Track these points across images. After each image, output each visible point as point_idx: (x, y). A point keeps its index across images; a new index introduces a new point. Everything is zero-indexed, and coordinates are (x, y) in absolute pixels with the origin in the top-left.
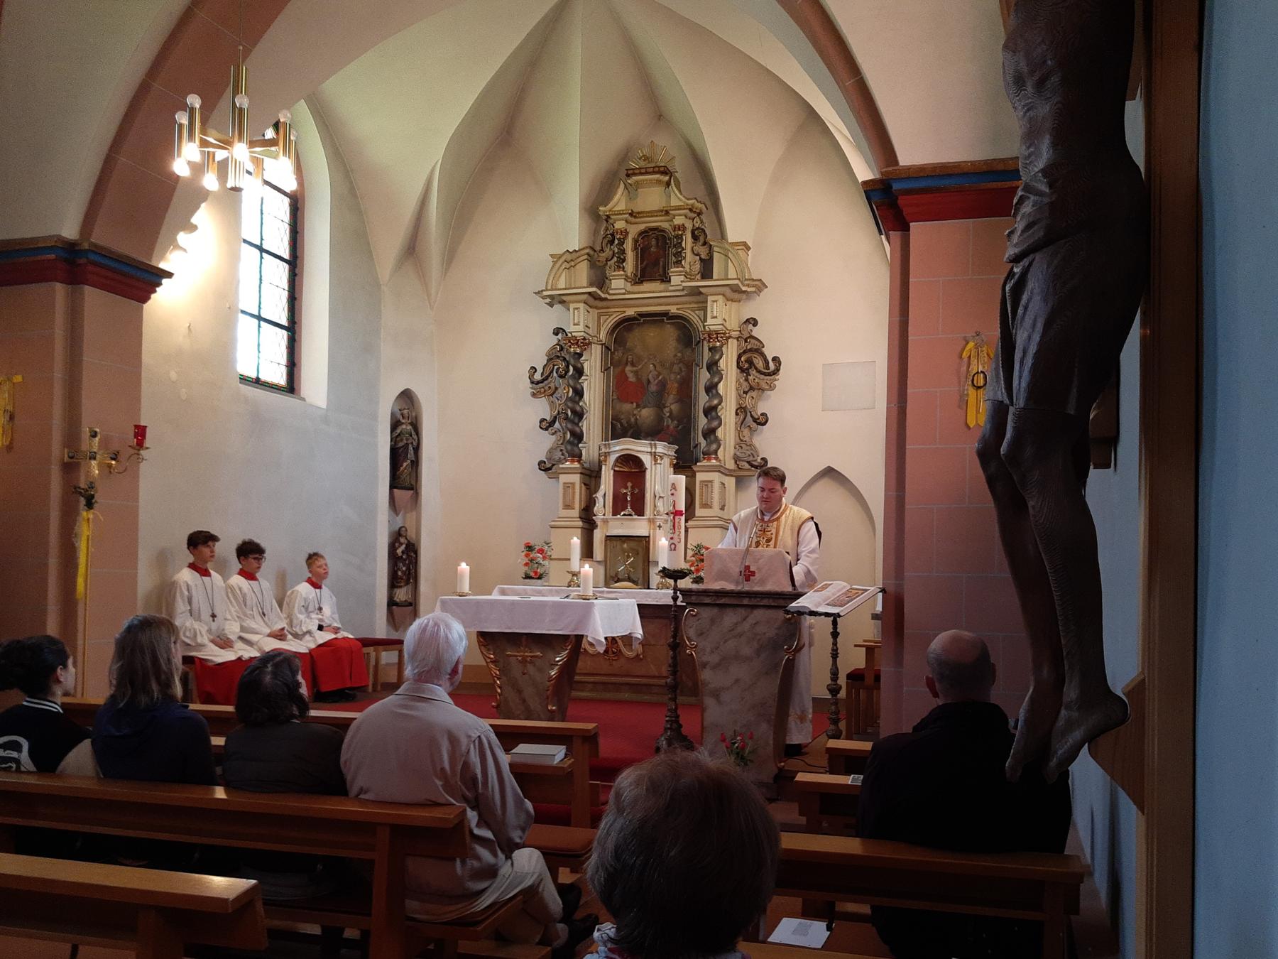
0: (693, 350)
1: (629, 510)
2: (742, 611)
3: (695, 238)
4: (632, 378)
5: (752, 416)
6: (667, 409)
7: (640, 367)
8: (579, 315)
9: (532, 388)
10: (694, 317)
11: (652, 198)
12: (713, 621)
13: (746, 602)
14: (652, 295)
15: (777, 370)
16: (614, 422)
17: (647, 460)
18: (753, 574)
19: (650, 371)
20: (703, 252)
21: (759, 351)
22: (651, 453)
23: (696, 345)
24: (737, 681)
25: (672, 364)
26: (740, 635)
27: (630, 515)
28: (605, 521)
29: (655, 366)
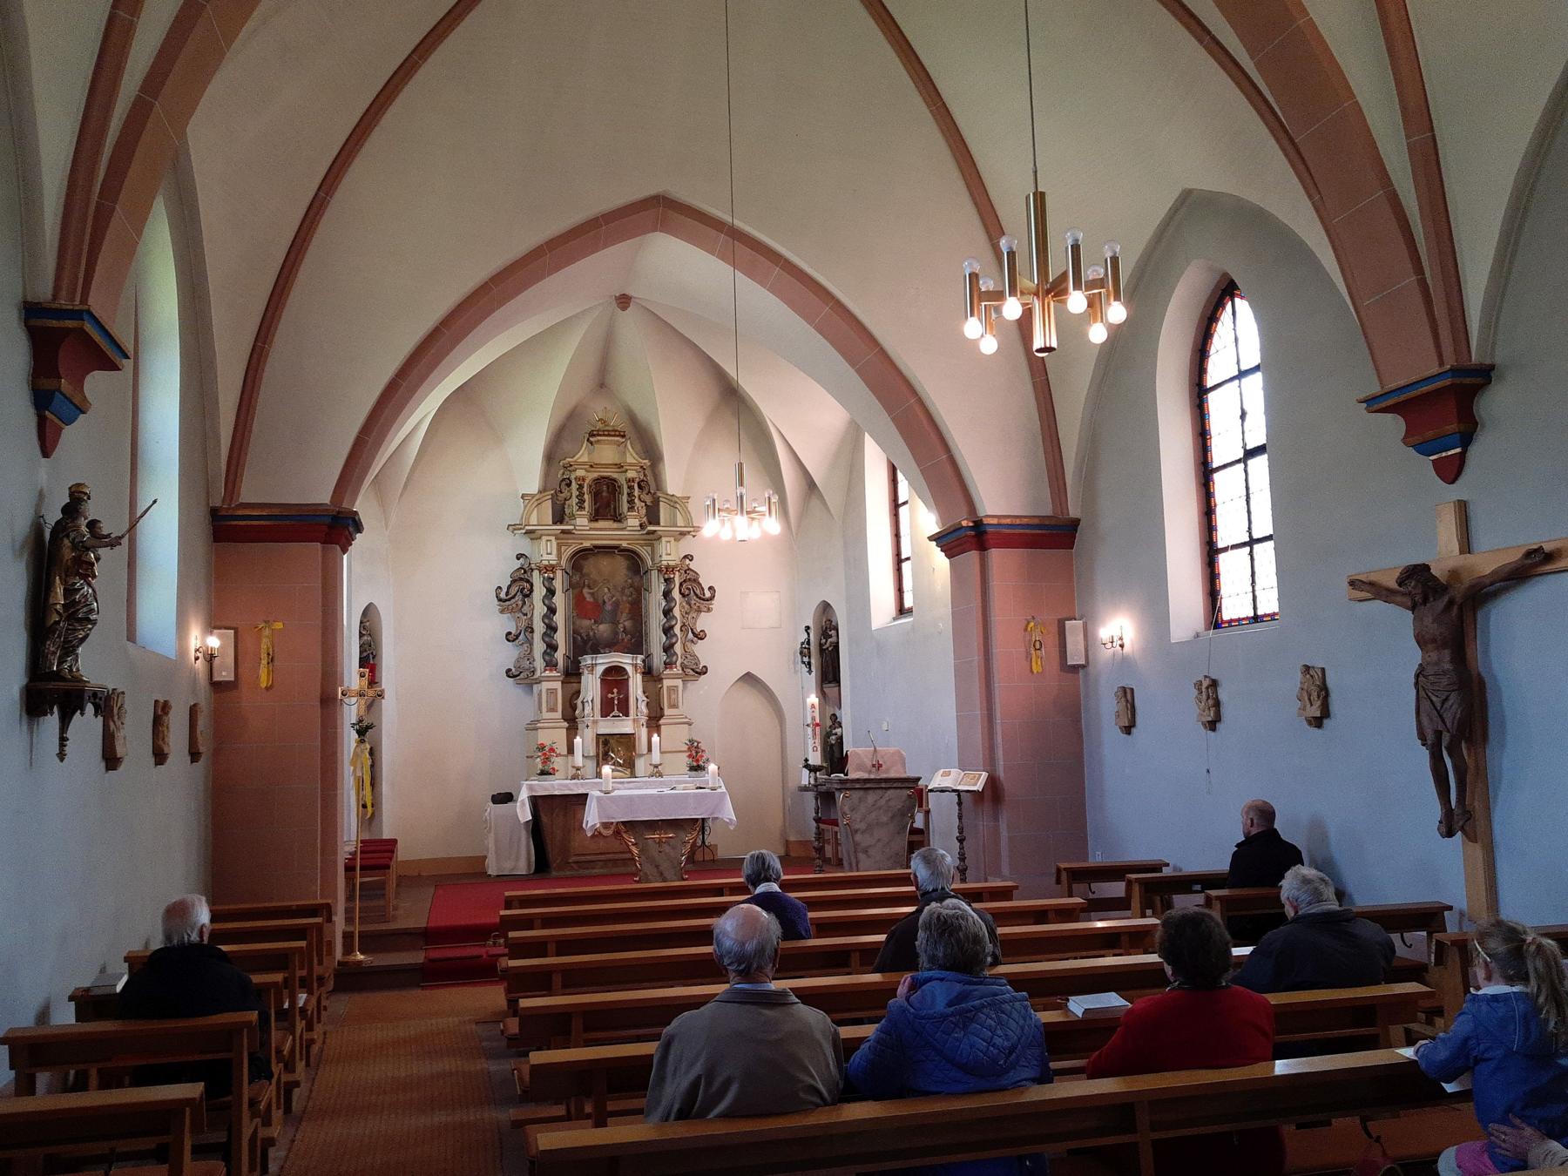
0: (642, 577)
1: (616, 712)
2: (880, 792)
3: (640, 487)
4: (589, 598)
5: (693, 633)
6: (622, 625)
7: (596, 589)
8: (551, 547)
9: (499, 605)
10: (644, 552)
11: (607, 453)
12: (860, 800)
13: (883, 785)
14: (607, 532)
15: (712, 598)
16: (575, 635)
17: (629, 669)
18: (880, 766)
19: (605, 593)
20: (648, 499)
21: (696, 581)
22: (632, 664)
23: (644, 574)
24: (879, 840)
25: (623, 589)
26: (880, 808)
27: (619, 716)
28: (595, 722)
29: (609, 589)
